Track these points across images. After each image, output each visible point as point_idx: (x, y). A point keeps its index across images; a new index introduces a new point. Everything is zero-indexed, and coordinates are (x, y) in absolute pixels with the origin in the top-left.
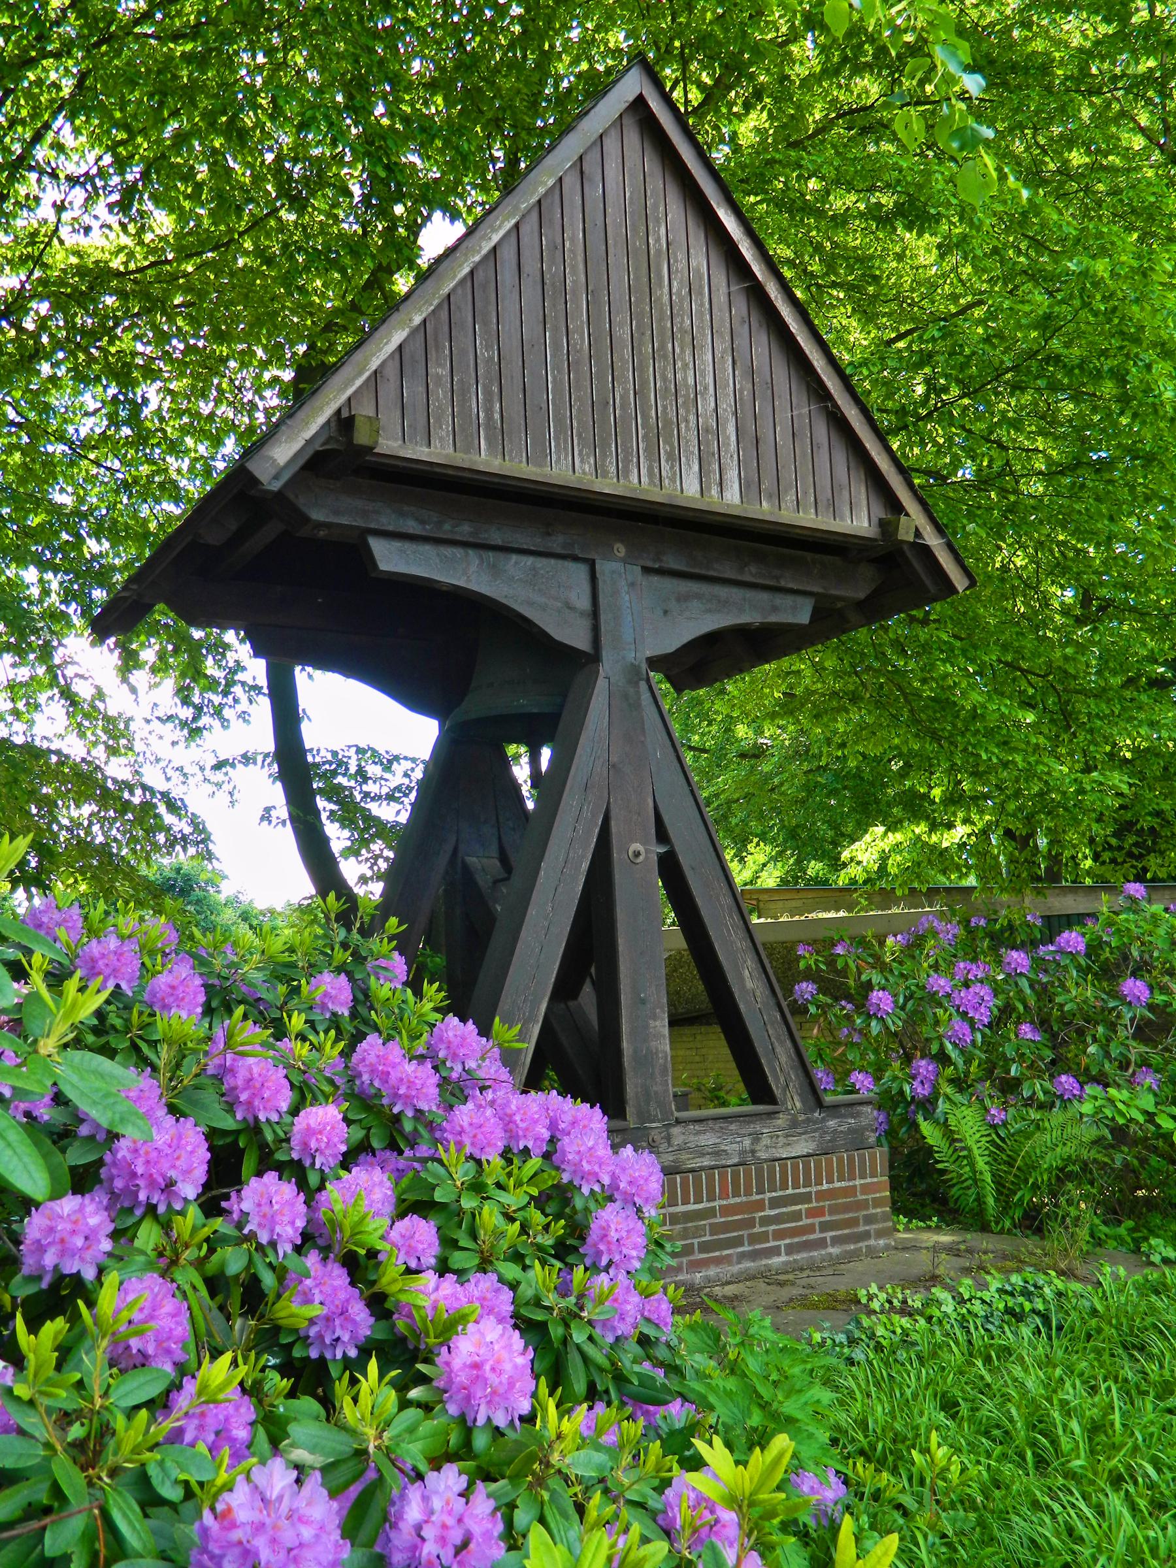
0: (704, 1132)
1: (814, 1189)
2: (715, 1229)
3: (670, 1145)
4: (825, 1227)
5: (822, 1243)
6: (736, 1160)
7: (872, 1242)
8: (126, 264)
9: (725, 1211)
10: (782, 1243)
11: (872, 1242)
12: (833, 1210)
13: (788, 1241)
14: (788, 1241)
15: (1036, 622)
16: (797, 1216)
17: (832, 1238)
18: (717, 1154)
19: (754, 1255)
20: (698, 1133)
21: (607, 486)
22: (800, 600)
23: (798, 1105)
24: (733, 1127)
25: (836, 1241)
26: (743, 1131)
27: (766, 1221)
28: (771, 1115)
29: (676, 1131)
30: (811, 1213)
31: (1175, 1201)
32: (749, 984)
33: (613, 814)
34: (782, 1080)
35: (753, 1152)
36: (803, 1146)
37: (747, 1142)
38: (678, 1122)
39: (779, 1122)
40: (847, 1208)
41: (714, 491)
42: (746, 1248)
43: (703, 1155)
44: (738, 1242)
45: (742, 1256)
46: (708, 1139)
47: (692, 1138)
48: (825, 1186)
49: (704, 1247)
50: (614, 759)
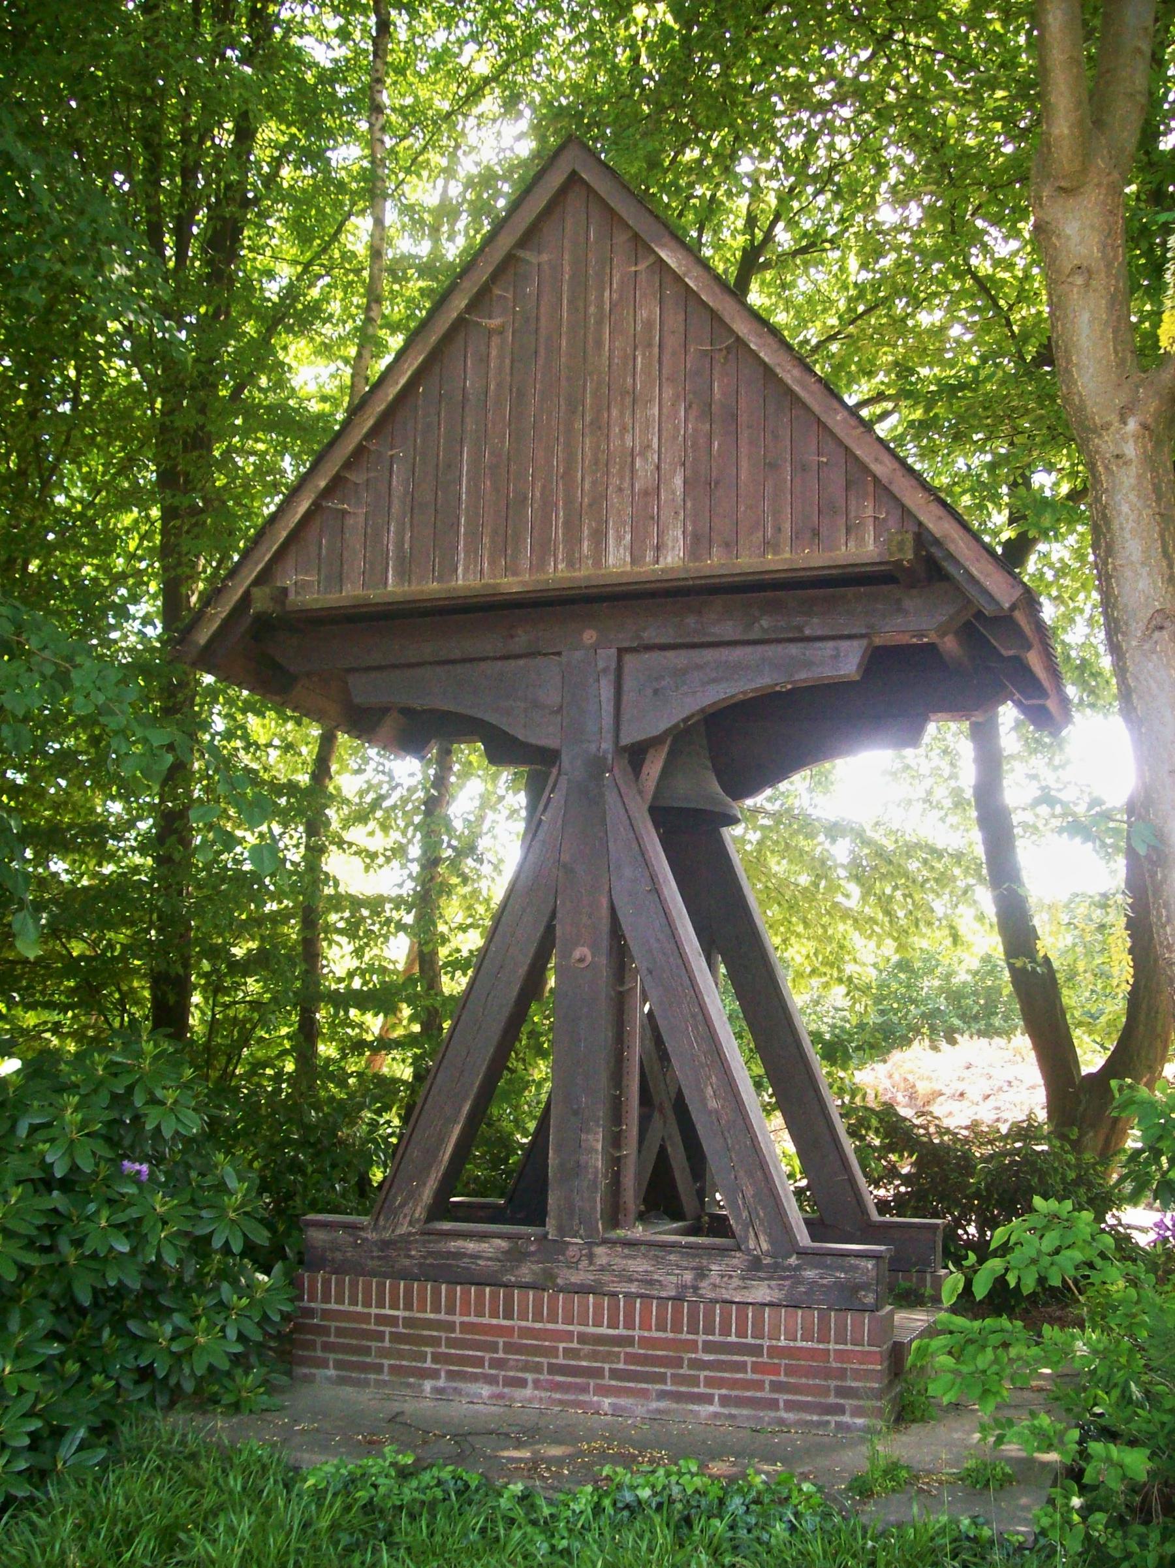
0: (633, 1257)
1: (766, 1343)
2: (631, 1358)
3: (591, 1263)
4: (777, 1387)
5: (773, 1404)
6: (673, 1293)
7: (846, 1419)
8: (829, 158)
9: (645, 1342)
10: (717, 1392)
11: (846, 1419)
12: (790, 1371)
13: (724, 1392)
14: (724, 1392)
15: (225, 868)
16: (741, 1367)
17: (786, 1402)
18: (651, 1283)
19: (677, 1397)
20: (626, 1257)
21: (512, 584)
22: (844, 645)
23: (765, 1246)
24: (672, 1257)
25: (790, 1406)
26: (685, 1264)
27: (697, 1364)
28: (723, 1251)
29: (600, 1250)
30: (756, 1368)
31: (1171, 1482)
32: (713, 1104)
33: (618, 904)
34: (745, 1214)
35: (696, 1288)
36: (762, 1292)
37: (688, 1277)
38: (604, 1242)
39: (735, 1261)
40: (809, 1372)
41: (650, 556)
42: (668, 1387)
43: (631, 1280)
44: (661, 1378)
45: (662, 1395)
46: (639, 1266)
47: (617, 1260)
48: (783, 1342)
49: (615, 1374)
50: (565, 857)
